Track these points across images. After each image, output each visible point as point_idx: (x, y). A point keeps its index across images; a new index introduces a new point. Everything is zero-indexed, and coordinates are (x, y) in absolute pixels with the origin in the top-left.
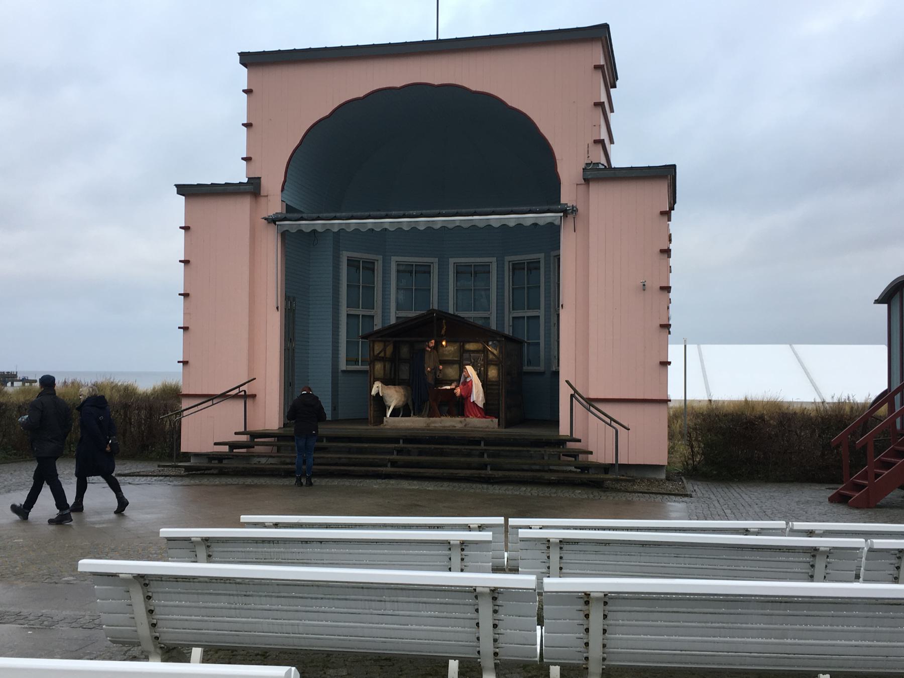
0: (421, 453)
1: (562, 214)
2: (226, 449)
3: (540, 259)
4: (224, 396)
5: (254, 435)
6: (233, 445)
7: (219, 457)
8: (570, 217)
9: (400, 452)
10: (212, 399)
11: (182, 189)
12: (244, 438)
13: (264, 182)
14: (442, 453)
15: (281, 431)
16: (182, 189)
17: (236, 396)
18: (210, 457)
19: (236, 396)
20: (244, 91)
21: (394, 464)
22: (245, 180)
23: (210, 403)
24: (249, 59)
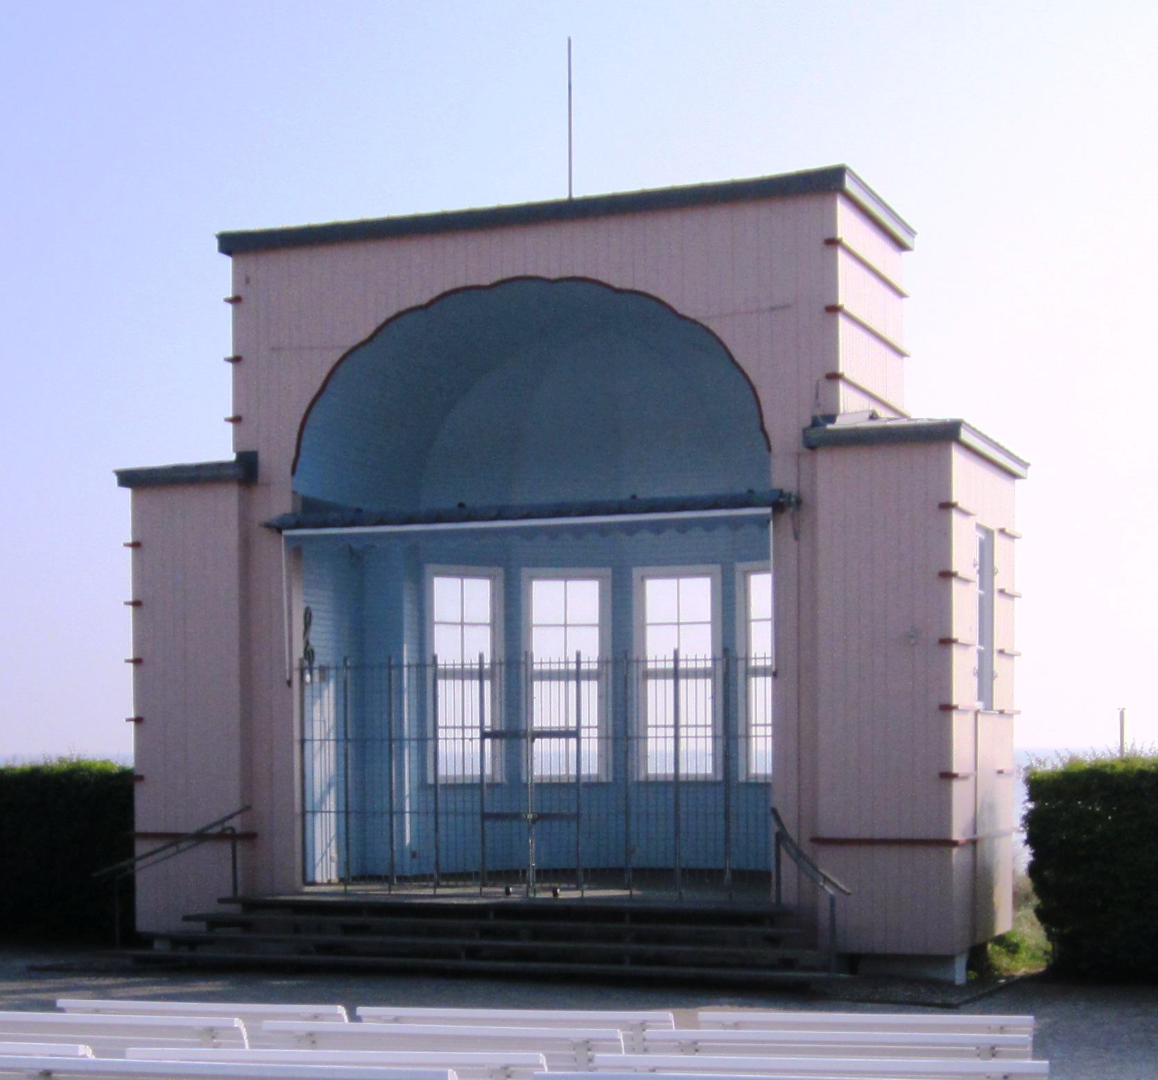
0: (536, 935)
1: (768, 510)
2: (201, 927)
3: (1025, 465)
4: (201, 837)
5: (251, 905)
6: (214, 922)
7: (192, 942)
8: (785, 518)
9: (487, 933)
10: (176, 843)
11: (128, 478)
12: (234, 909)
13: (263, 458)
14: (662, 939)
15: (1038, 806)
16: (128, 478)
17: (221, 836)
18: (176, 941)
19: (221, 836)
20: (228, 301)
21: (638, 959)
22: (231, 457)
23: (171, 851)
24: (232, 244)
